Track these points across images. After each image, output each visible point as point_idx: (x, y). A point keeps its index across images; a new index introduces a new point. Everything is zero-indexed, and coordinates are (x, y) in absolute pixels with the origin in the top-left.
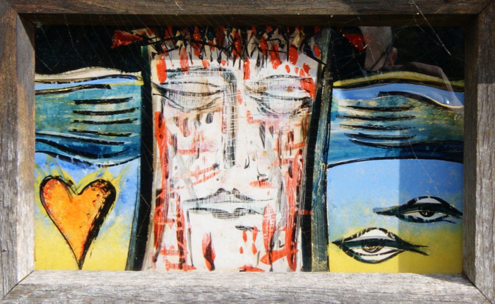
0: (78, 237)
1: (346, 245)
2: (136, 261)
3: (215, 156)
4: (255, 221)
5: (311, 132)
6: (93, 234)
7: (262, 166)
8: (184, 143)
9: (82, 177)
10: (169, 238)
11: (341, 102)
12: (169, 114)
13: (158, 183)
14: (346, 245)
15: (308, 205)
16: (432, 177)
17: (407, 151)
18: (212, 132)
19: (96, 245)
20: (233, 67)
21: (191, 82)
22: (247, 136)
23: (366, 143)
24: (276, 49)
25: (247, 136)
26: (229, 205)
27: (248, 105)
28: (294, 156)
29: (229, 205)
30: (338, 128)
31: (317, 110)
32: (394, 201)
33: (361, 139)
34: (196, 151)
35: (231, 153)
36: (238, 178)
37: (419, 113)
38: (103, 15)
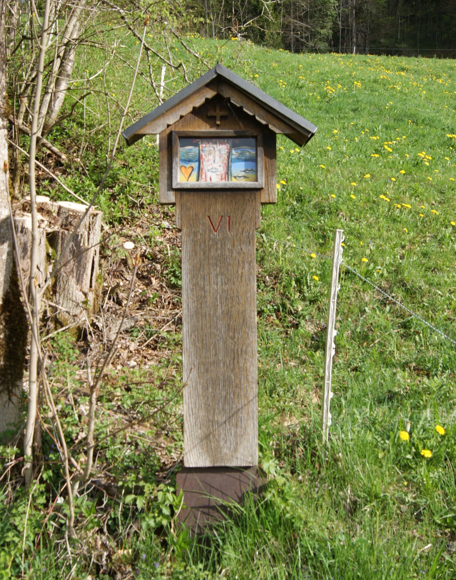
0: (187, 176)
1: (235, 177)
2: (198, 180)
3: (212, 162)
4: (219, 173)
5: (228, 157)
6: (190, 176)
7: (220, 163)
8: (206, 159)
9: (188, 166)
10: (204, 176)
11: (234, 152)
12: (203, 154)
13: (201, 166)
14: (235, 177)
15: (228, 170)
16: (251, 165)
17: (246, 160)
18: (211, 157)
19: (190, 178)
20: (215, 146)
21: (207, 149)
22: (217, 158)
23: (238, 159)
24: (55, 476)
25: (217, 158)
26: (214, 170)
27: (217, 153)
28: (226, 162)
29: (214, 170)
30: (233, 157)
31: (229, 153)
32: (244, 169)
33: (238, 159)
34: (208, 161)
35: (214, 161)
36: (216, 165)
37: (248, 154)
38: (146, 125)
